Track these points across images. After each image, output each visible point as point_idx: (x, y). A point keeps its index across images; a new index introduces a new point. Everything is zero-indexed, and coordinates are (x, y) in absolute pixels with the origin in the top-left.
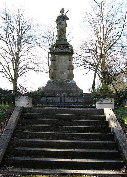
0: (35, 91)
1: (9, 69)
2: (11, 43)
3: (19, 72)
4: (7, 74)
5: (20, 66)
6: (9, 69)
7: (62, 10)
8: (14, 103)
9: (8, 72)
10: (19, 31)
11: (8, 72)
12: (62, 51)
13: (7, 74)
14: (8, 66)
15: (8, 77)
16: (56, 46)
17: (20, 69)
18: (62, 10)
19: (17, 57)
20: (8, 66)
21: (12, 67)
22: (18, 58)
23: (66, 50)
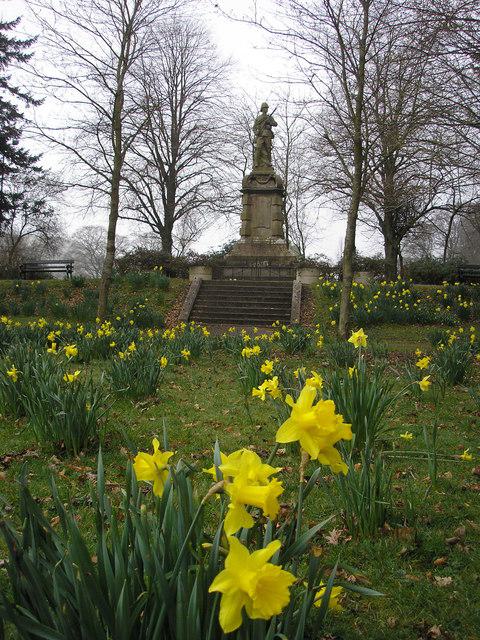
0: (228, 249)
1: (151, 201)
2: (156, 138)
3: (177, 208)
4: (147, 214)
5: (179, 193)
6: (151, 201)
7: (265, 108)
8: (309, 264)
9: (150, 209)
10: (176, 107)
11: (150, 209)
12: (264, 187)
13: (147, 214)
14: (150, 193)
15: (152, 222)
16: (252, 178)
17: (180, 200)
18: (265, 108)
19: (171, 166)
20: (150, 193)
21: (160, 196)
22: (174, 172)
23: (272, 186)
